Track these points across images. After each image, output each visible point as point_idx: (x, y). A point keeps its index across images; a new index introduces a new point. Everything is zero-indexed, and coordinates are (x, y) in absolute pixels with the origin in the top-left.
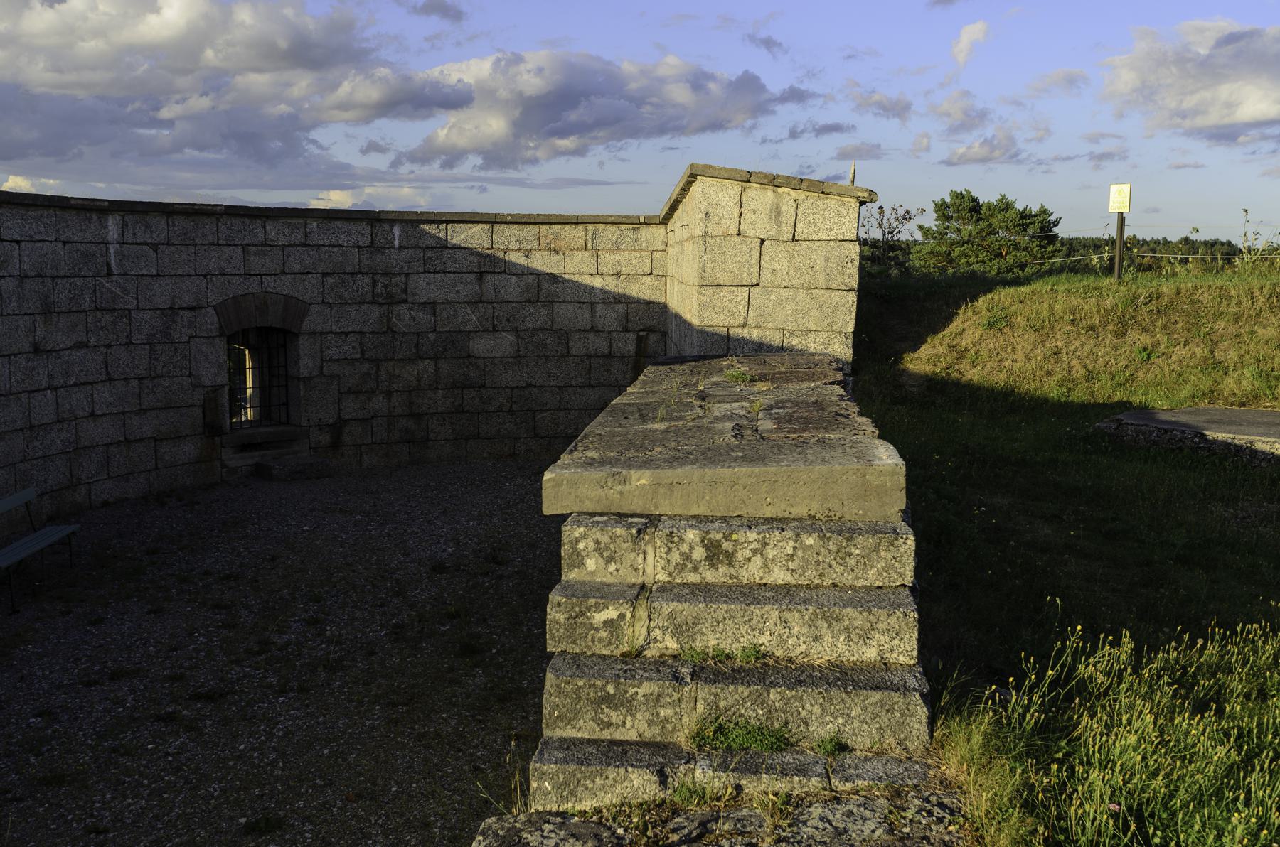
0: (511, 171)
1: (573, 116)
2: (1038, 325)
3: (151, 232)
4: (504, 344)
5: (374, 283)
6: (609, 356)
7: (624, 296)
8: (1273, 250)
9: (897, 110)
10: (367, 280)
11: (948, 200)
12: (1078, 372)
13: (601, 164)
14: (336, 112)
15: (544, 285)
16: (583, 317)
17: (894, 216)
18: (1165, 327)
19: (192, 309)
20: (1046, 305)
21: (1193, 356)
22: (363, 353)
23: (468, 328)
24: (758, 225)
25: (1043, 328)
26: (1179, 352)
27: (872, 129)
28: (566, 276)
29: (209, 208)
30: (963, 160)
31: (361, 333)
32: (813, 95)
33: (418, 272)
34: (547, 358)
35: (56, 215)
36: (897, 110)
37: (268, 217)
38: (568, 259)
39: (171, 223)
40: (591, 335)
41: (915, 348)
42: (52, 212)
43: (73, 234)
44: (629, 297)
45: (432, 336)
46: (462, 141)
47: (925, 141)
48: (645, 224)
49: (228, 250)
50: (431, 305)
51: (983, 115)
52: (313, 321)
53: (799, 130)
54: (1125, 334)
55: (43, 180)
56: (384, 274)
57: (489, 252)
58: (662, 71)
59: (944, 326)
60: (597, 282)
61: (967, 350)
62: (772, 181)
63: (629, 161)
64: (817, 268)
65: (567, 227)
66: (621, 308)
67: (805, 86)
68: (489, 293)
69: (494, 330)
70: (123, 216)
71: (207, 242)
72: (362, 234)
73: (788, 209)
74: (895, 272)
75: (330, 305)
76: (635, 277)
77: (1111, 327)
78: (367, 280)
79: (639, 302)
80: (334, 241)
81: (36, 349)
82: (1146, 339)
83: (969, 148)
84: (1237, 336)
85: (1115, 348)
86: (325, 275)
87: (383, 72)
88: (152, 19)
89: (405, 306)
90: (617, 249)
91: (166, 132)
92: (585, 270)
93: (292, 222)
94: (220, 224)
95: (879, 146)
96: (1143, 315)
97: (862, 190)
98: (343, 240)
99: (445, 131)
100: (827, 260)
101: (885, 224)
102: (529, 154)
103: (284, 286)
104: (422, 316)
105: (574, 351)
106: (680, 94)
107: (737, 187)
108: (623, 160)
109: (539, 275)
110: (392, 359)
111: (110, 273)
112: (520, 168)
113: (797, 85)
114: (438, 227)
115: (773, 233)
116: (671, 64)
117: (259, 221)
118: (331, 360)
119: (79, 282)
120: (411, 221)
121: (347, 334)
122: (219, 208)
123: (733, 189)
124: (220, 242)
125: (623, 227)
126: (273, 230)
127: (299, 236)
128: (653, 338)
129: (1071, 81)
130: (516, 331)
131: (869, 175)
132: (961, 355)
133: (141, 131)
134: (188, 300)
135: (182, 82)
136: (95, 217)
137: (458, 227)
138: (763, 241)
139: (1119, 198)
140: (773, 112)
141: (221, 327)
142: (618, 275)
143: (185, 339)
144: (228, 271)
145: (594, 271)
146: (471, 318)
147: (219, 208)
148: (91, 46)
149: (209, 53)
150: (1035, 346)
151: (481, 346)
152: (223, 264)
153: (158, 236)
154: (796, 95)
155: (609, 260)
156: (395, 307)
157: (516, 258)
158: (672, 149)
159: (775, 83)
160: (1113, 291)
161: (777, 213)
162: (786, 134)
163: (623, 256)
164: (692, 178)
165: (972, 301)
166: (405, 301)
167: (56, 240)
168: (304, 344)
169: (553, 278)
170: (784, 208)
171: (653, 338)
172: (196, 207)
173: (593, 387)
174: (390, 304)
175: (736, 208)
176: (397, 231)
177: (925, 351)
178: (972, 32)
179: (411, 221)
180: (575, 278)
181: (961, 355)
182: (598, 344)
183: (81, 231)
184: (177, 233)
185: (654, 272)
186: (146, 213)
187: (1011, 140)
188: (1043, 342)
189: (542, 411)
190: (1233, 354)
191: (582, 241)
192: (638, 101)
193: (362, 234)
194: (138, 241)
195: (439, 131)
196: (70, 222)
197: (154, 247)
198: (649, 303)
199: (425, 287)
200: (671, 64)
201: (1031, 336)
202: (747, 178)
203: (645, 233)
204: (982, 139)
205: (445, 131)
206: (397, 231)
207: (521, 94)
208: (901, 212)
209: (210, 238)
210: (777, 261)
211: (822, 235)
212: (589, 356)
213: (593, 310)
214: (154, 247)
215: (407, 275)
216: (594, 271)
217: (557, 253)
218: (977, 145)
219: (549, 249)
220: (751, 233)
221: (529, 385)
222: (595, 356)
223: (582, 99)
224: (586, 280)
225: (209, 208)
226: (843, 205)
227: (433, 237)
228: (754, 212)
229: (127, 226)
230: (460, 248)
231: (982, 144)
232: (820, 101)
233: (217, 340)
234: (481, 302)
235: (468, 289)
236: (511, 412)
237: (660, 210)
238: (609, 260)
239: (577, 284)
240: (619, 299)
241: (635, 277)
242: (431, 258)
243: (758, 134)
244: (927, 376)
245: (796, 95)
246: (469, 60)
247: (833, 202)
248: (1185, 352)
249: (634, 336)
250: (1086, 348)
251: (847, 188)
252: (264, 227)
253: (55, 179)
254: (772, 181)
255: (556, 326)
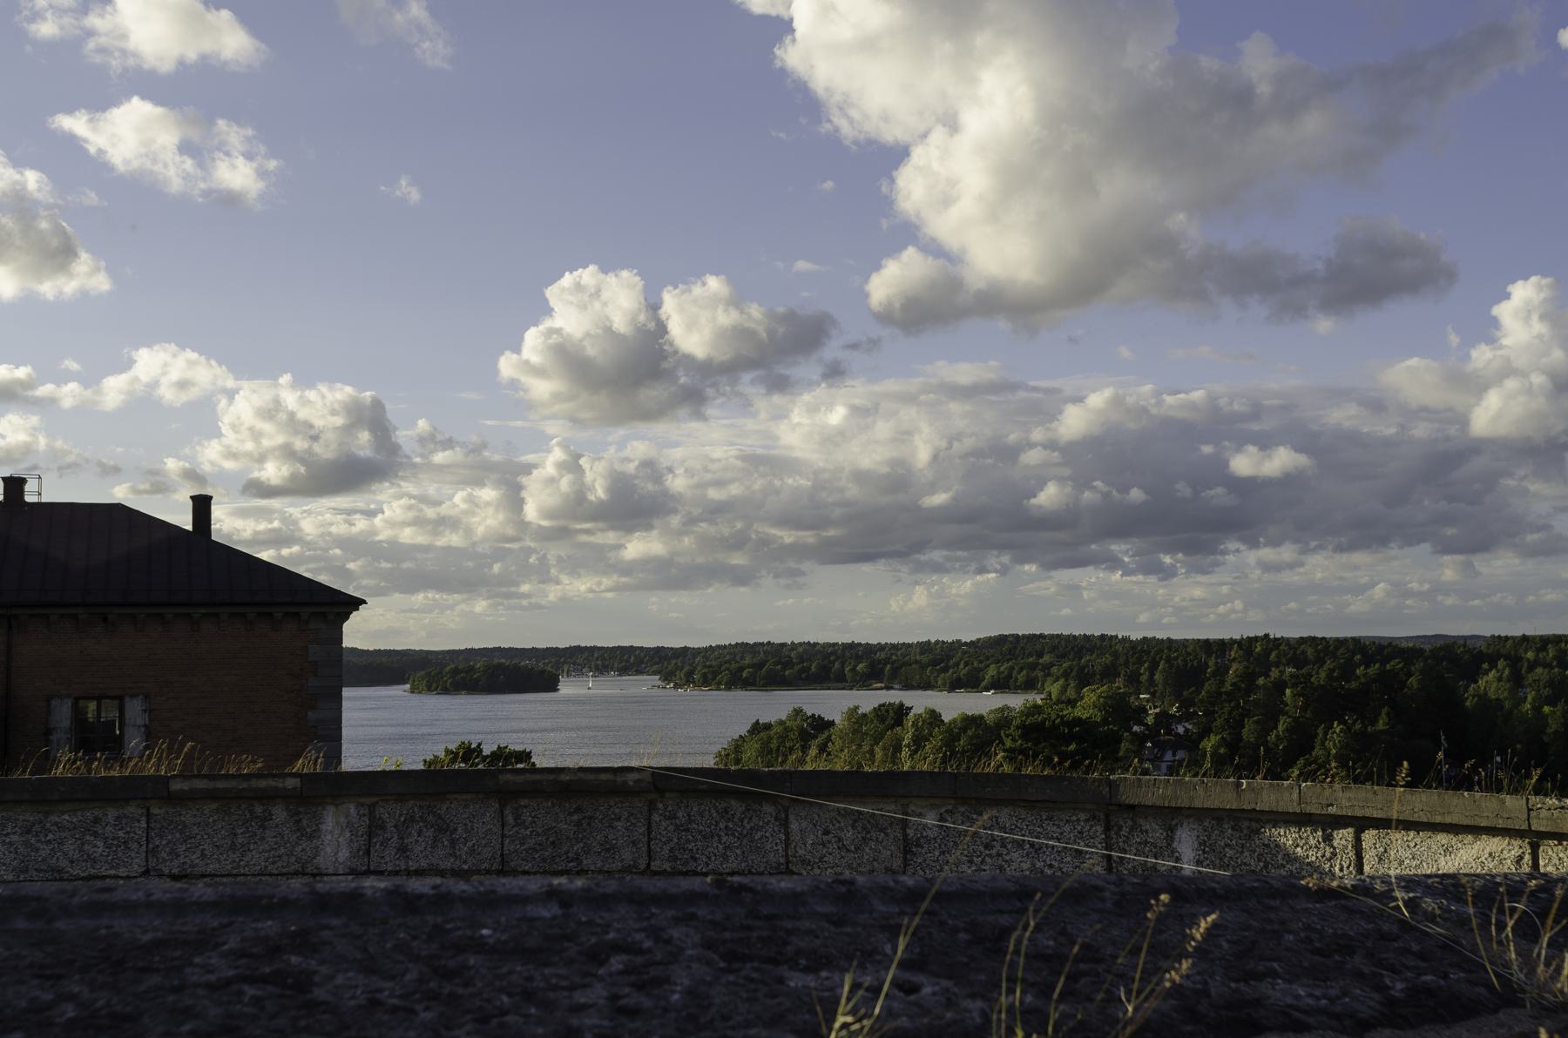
3: (453, 843)
29: (603, 777)
35: (149, 816)
39: (510, 819)
42: (132, 810)
43: (203, 855)
70: (372, 807)
71: (618, 865)
94: (656, 817)
112: (206, 444)
114: (1328, 839)
117: (768, 809)
122: (635, 776)
124: (655, 866)
136: (280, 813)
147: (635, 776)
153: (472, 851)
167: (146, 873)
172: (565, 777)
183: (233, 847)
184: (531, 842)
194: (413, 866)
196: (195, 830)
209: (627, 855)
225: (603, 777)
229: (383, 827)
244: (115, 106)
252: (785, 824)
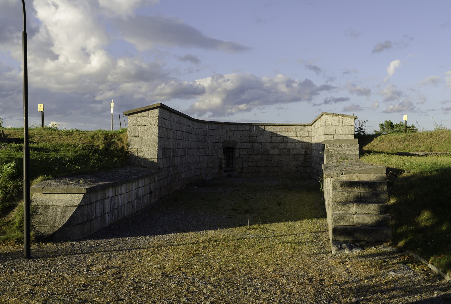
0: (222, 117)
1: (244, 97)
2: (388, 141)
4: (276, 151)
5: (250, 138)
6: (299, 154)
7: (302, 141)
8: (449, 131)
9: (366, 93)
10: (248, 137)
11: (384, 124)
12: (395, 148)
13: (255, 115)
14: (158, 97)
15: (285, 139)
16: (293, 146)
17: (362, 122)
18: (412, 141)
19: (218, 143)
20: (390, 138)
21: (416, 145)
22: (247, 153)
23: (268, 148)
24: (335, 123)
25: (389, 142)
26: (413, 145)
27: (355, 99)
28: (289, 137)
30: (392, 111)
31: (247, 149)
32: (333, 88)
33: (259, 136)
34: (285, 155)
36: (366, 93)
37: (231, 124)
38: (290, 133)
40: (295, 150)
41: (365, 146)
44: (303, 142)
45: (261, 150)
46: (204, 107)
47: (377, 104)
48: (307, 125)
49: (224, 131)
50: (261, 143)
51: (399, 94)
52: (238, 146)
53: (328, 100)
54: (404, 142)
55: (62, 123)
56: (252, 136)
57: (273, 132)
58: (276, 80)
59: (371, 142)
60: (296, 138)
61: (375, 146)
62: (338, 115)
63: (265, 113)
64: (347, 131)
65: (290, 126)
66: (301, 144)
67: (329, 83)
68: (273, 141)
69: (274, 149)
72: (248, 128)
73: (341, 120)
74: (362, 134)
75: (241, 143)
76: (305, 137)
77: (402, 141)
78: (248, 137)
79: (305, 142)
80: (243, 130)
81: (198, 148)
82: (408, 143)
83: (394, 106)
84: (424, 142)
85: (402, 144)
86: (241, 136)
87: (173, 82)
88: (88, 66)
89: (256, 143)
90: (301, 131)
91: (100, 105)
92: (293, 136)
93: (235, 125)
95: (358, 106)
96: (408, 139)
97: (355, 116)
98: (244, 129)
99: (198, 103)
100: (348, 129)
101: (360, 124)
102: (229, 111)
103: (233, 138)
104: (259, 145)
105: (291, 153)
106: (283, 88)
107: (331, 116)
108: (263, 113)
109: (284, 137)
110: (253, 154)
111: (207, 135)
113: (326, 84)
115: (338, 124)
116: (280, 77)
118: (241, 154)
119: (203, 136)
120: (257, 125)
121: (244, 149)
123: (331, 117)
125: (302, 126)
126: (232, 127)
127: (236, 129)
128: (308, 150)
129: (434, 81)
130: (278, 149)
131: (356, 114)
132: (374, 146)
133: (91, 105)
134: (217, 141)
135: (102, 87)
137: (267, 126)
138: (336, 126)
139: (405, 118)
140: (319, 94)
141: (222, 147)
142: (301, 137)
143: (217, 148)
144: (224, 135)
145: (296, 136)
146: (269, 146)
148: (69, 75)
149: (109, 77)
150: (388, 144)
151: (271, 152)
152: (223, 134)
154: (326, 88)
155: (299, 133)
156: (254, 143)
157: (279, 133)
158: (282, 108)
159: (318, 82)
160: (403, 135)
161: (339, 121)
162: (323, 102)
163: (302, 133)
164: (323, 114)
165: (376, 137)
166: (256, 142)
168: (237, 151)
169: (287, 137)
170: (340, 120)
171: (308, 150)
173: (295, 161)
174: (253, 143)
175: (331, 120)
176: (255, 127)
177: (367, 146)
178: (394, 64)
179: (258, 125)
180: (291, 137)
181: (374, 146)
182: (297, 152)
185: (309, 136)
186: (212, 123)
187: (411, 104)
188: (389, 144)
189: (284, 166)
190: (422, 145)
191: (293, 129)
192: (268, 91)
193: (248, 128)
195: (196, 103)
197: (213, 130)
198: (308, 143)
199: (260, 139)
200: (280, 77)
201: (387, 143)
202: (333, 115)
203: (307, 127)
204: (399, 103)
205: (198, 103)
206: (255, 127)
207: (225, 89)
208: (363, 121)
209: (221, 129)
210: (339, 130)
211: (348, 125)
212: (294, 154)
213: (295, 144)
214: (213, 130)
215: (256, 137)
216: (296, 136)
217: (288, 132)
218: (397, 105)
219: (286, 131)
220: (334, 125)
221: (281, 161)
222: (296, 154)
223: (245, 90)
224: (294, 138)
226: (351, 119)
227: (262, 129)
228: (335, 121)
230: (267, 131)
231: (399, 105)
232: (336, 90)
233: (222, 149)
234: (271, 142)
235: (269, 140)
236: (277, 166)
237: (311, 122)
238: (299, 133)
239: (292, 139)
240: (301, 142)
241: (305, 137)
242: (261, 133)
243: (313, 102)
245: (326, 88)
246: (207, 78)
247: (349, 119)
248: (414, 145)
249: (304, 150)
250: (397, 145)
251: (352, 116)
253: (65, 122)
254: (338, 115)
255: (287, 148)
